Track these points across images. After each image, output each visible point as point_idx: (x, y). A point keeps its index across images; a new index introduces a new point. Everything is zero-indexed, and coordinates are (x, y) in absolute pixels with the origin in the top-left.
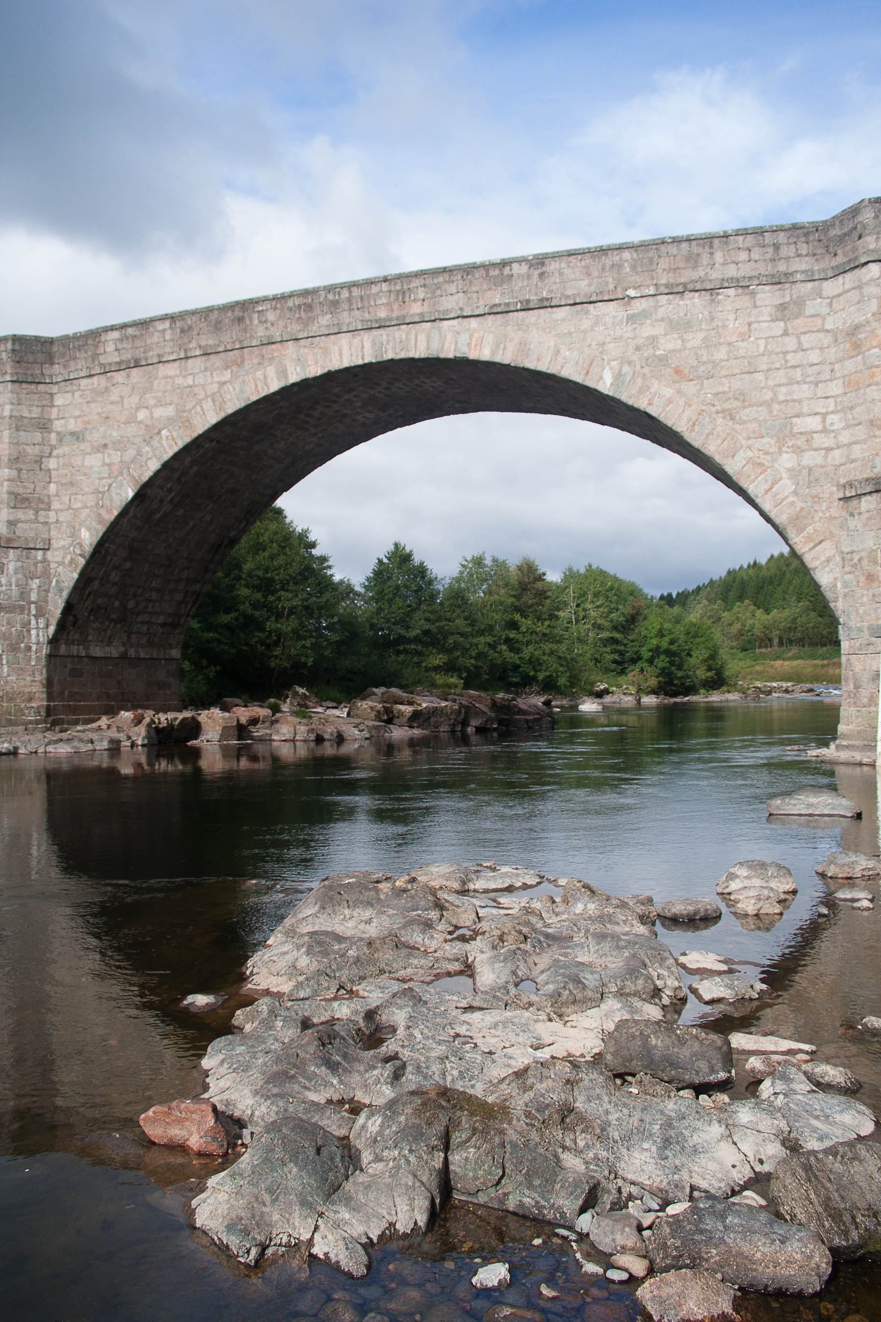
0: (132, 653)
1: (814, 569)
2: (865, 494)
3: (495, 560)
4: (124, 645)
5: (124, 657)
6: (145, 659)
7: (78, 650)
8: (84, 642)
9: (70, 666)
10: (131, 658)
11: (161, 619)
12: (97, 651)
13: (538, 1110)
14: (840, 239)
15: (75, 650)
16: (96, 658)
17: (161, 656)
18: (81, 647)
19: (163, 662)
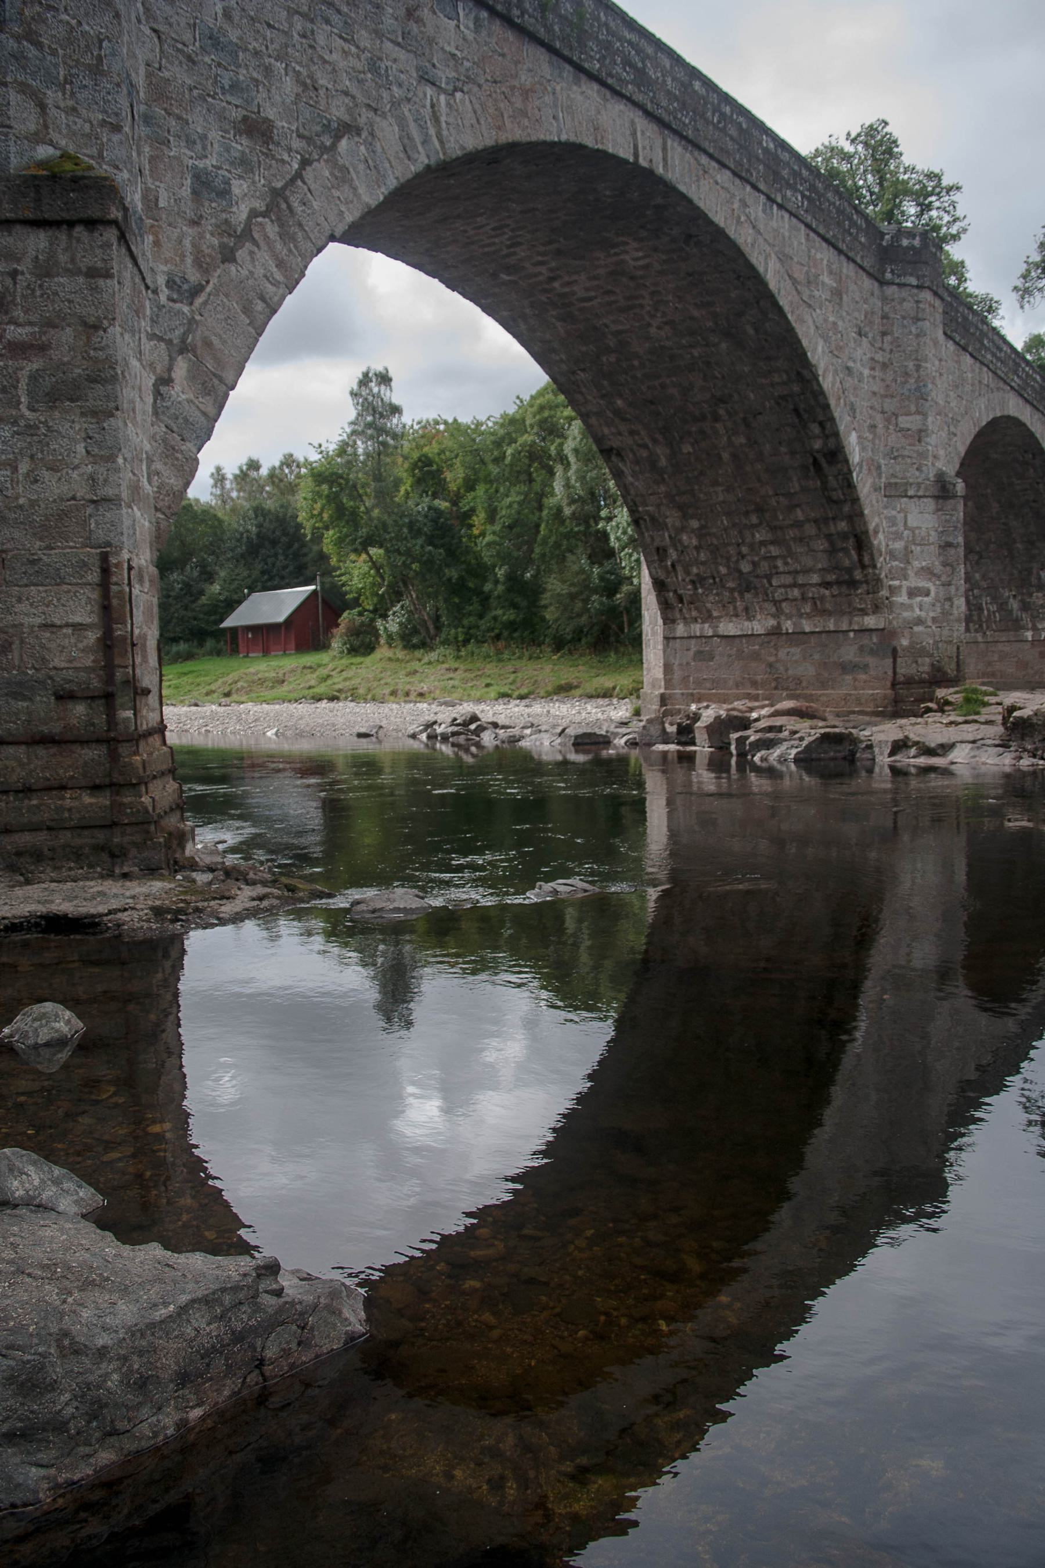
0: (788, 626)
1: (462, 148)
2: (630, 100)
3: (810, 1307)
4: (774, 616)
5: (775, 632)
6: (813, 633)
7: (702, 629)
8: (708, 617)
9: (694, 649)
10: (787, 634)
11: (815, 578)
12: (729, 627)
13: (170, 284)
14: (7, 831)
15: (696, 629)
16: (734, 637)
17: (845, 627)
18: (706, 625)
19: (852, 634)
